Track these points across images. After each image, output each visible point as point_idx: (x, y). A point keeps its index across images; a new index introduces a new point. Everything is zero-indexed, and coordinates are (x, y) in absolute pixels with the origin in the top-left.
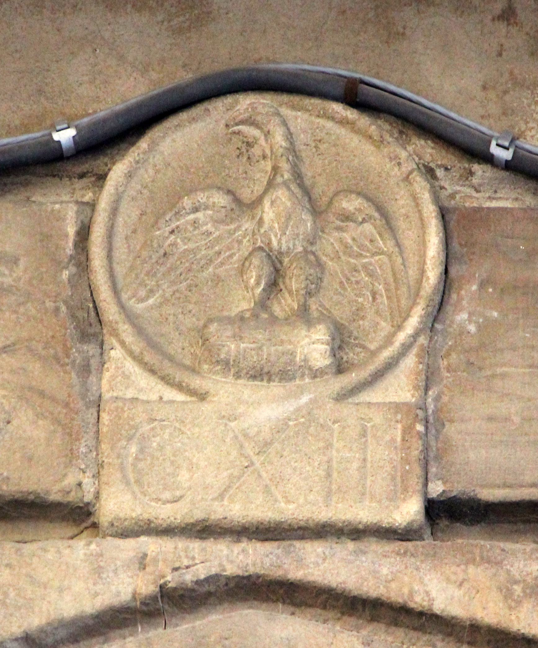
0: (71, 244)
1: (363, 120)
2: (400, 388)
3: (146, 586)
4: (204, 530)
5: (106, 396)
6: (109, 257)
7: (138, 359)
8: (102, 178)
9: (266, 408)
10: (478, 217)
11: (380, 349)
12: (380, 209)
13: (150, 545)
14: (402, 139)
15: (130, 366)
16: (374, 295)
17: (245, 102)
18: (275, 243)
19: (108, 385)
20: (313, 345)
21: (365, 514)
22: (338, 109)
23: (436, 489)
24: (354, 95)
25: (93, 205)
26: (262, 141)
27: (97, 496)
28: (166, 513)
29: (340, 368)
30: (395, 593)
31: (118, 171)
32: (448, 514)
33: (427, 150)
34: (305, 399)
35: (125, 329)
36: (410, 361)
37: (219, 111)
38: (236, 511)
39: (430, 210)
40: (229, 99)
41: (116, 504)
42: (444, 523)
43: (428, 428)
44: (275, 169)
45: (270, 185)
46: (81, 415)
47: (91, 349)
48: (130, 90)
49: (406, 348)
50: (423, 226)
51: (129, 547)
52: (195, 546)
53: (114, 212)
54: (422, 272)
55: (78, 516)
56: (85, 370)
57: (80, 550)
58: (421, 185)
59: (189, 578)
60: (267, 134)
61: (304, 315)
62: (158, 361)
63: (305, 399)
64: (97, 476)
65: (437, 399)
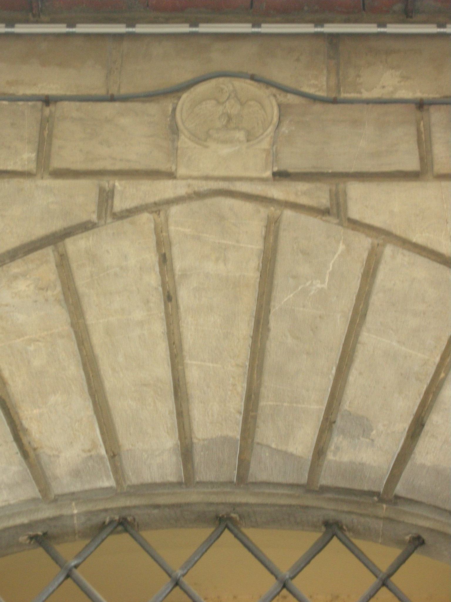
0: (170, 112)
1: (256, 84)
2: (265, 144)
3: (190, 191)
4: (207, 178)
5: (179, 146)
6: (181, 114)
7: (189, 139)
8: (179, 98)
9: (225, 150)
10: (289, 106)
11: (260, 136)
12: (260, 103)
13: (190, 181)
14: (267, 88)
15: (186, 140)
16: (258, 124)
17: (221, 80)
18: (229, 112)
19: (179, 144)
20: (241, 135)
21: (254, 174)
22: (249, 81)
23: (276, 169)
24: (253, 78)
25: (177, 104)
26: (226, 88)
27: (176, 170)
28: (195, 174)
29: (248, 141)
30: (263, 194)
31: (185, 96)
32: (281, 175)
33: (274, 90)
34: (237, 148)
35: (186, 133)
36: (268, 139)
37: (213, 83)
38: (216, 174)
39: (274, 103)
40: (217, 79)
41: (182, 171)
42: (277, 177)
43: (274, 155)
44: (230, 95)
45: (228, 98)
46: (174, 153)
47: (175, 136)
48: (188, 76)
49: (267, 135)
50: (273, 107)
51: (184, 182)
52: (204, 183)
53: (183, 104)
54: (272, 118)
55: (171, 175)
56: (173, 141)
57: (170, 183)
58: (272, 98)
59: (202, 189)
60: (228, 87)
61: (237, 128)
62: (195, 137)
63: (237, 148)
64: (176, 165)
65: (277, 148)
